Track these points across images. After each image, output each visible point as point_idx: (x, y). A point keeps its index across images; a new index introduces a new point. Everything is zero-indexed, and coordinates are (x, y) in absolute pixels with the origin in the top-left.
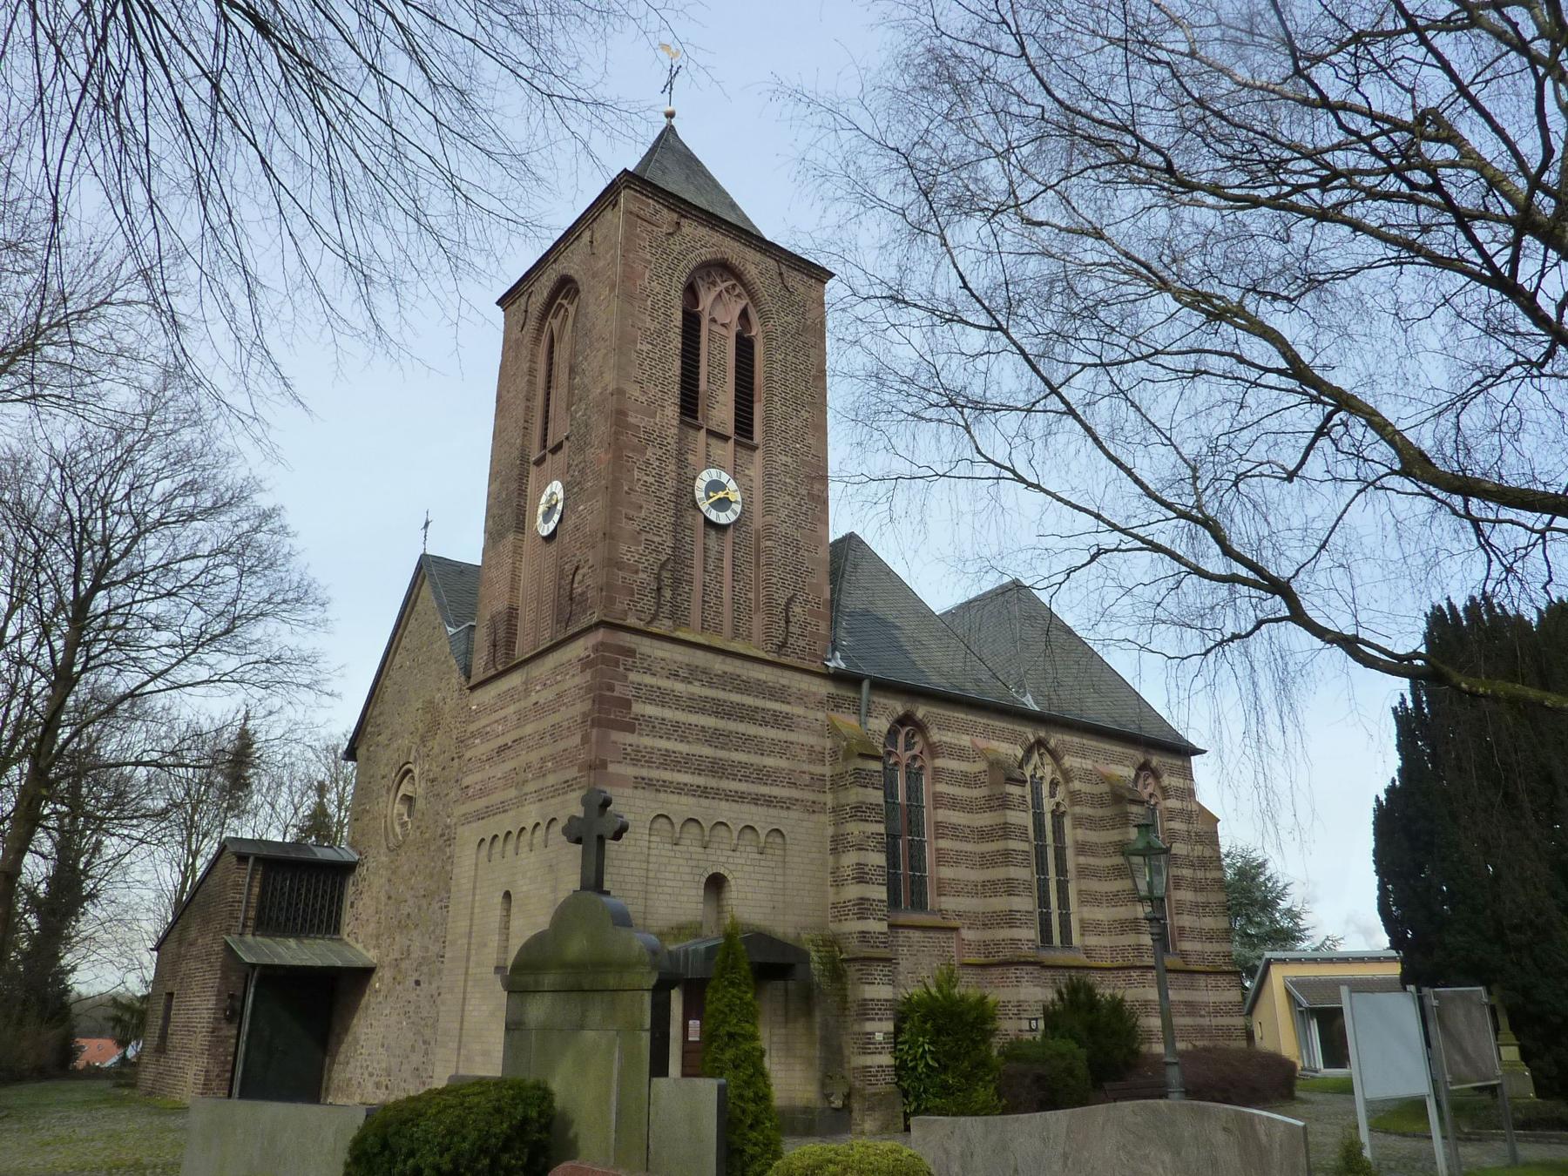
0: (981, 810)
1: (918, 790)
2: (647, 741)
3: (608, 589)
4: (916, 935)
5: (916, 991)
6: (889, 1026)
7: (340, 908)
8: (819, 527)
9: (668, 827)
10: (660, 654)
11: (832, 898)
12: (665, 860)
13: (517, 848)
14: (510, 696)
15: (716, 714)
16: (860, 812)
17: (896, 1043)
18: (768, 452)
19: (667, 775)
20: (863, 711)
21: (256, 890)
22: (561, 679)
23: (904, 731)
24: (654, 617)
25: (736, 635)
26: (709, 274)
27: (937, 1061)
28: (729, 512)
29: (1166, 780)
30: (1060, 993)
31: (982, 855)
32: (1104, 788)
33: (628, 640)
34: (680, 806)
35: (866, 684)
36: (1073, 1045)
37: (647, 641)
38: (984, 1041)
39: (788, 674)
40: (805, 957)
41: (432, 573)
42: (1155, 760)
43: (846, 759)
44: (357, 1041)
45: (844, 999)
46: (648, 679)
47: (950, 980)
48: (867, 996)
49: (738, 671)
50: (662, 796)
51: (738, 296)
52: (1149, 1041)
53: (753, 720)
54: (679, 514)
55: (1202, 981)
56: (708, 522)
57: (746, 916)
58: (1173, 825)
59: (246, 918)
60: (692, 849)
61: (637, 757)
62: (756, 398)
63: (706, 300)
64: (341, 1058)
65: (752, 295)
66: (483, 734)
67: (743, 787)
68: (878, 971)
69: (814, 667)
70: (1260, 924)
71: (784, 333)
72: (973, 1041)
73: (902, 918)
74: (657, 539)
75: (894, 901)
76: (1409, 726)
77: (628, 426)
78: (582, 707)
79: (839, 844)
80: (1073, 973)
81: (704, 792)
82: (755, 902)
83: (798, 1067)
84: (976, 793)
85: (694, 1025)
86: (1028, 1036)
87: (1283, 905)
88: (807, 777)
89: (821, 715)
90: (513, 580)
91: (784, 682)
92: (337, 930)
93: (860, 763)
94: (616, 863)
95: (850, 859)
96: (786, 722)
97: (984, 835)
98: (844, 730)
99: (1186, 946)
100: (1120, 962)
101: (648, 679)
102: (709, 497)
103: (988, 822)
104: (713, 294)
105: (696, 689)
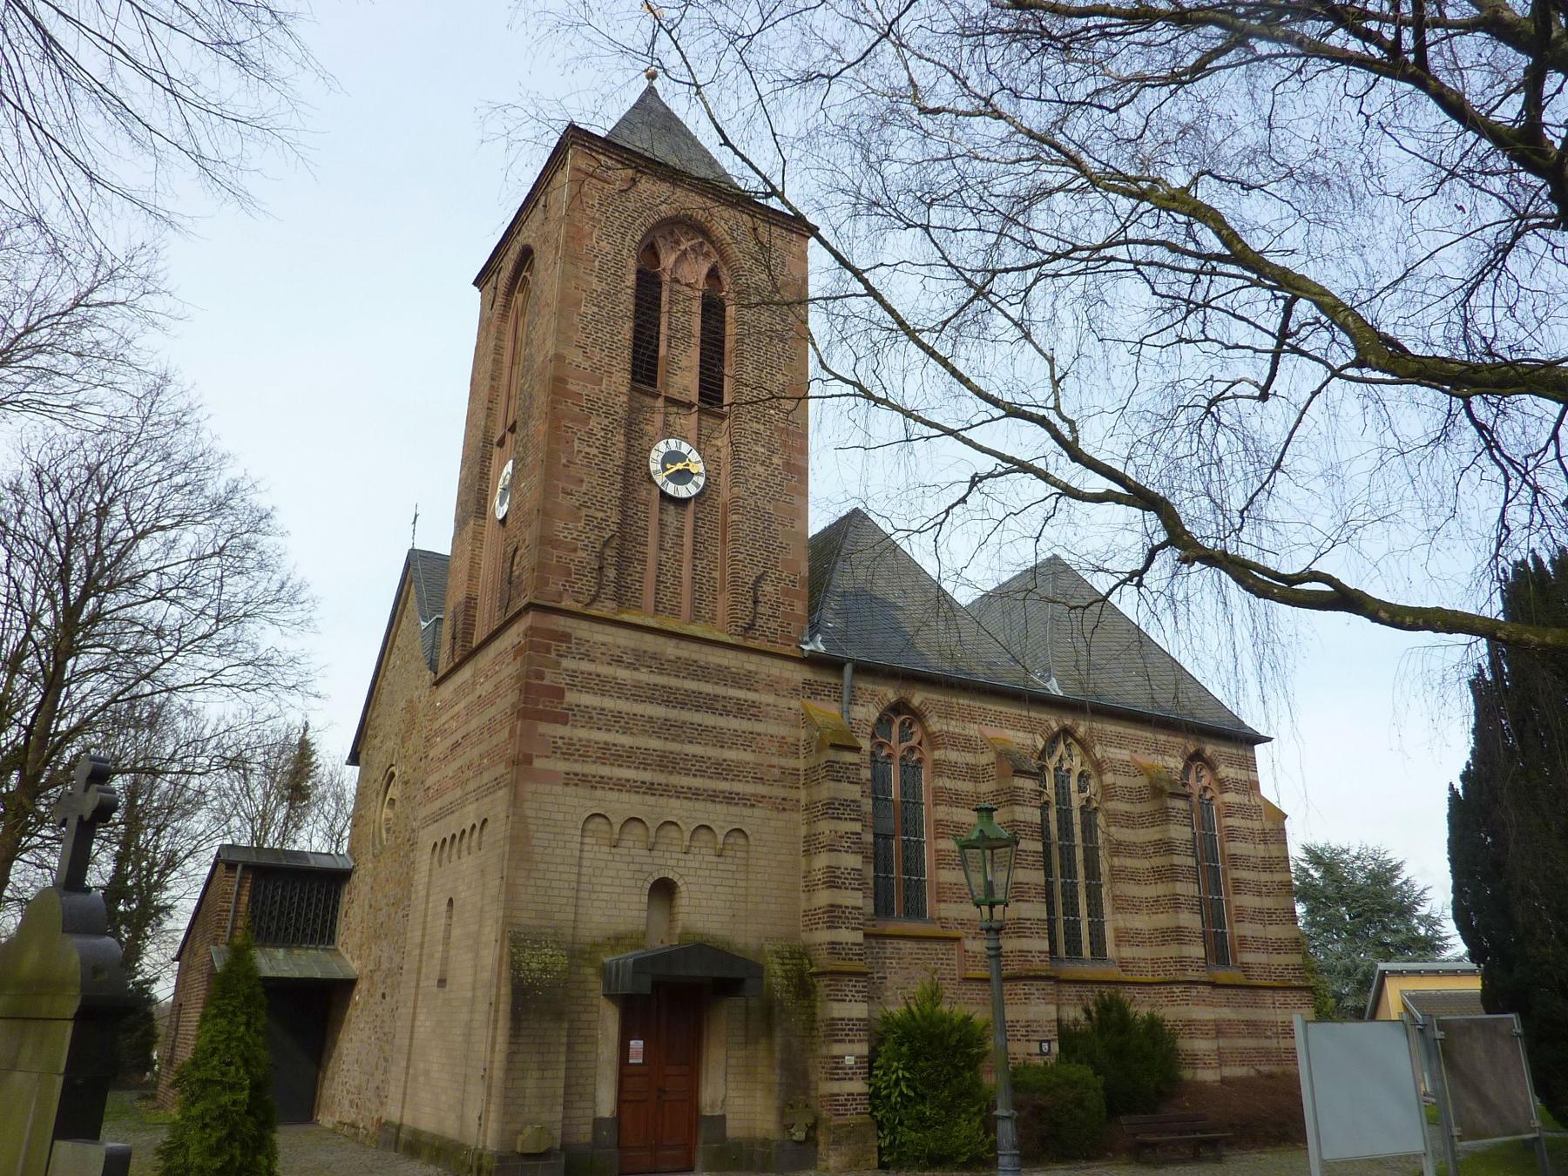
1: (917, 786)
2: (583, 733)
3: (541, 568)
4: (907, 946)
5: (897, 1010)
6: (864, 1049)
7: (334, 917)
9: (606, 828)
10: (600, 638)
11: (804, 906)
12: (602, 864)
13: (459, 851)
14: (461, 692)
15: (666, 703)
16: (834, 809)
17: (871, 1068)
19: (605, 771)
20: (846, 698)
21: (245, 899)
22: (496, 671)
23: (898, 721)
24: (595, 599)
25: (696, 616)
26: (672, 233)
27: (914, 1090)
28: (690, 485)
29: (1224, 771)
30: (1087, 1011)
32: (1142, 781)
33: (562, 623)
34: (621, 805)
35: (848, 669)
36: (1086, 1072)
37: (585, 625)
39: (755, 658)
41: (419, 567)
42: (1209, 749)
43: (819, 751)
44: (341, 1055)
45: (812, 1018)
46: (586, 666)
47: (935, 996)
48: (836, 1015)
49: (695, 656)
50: (599, 793)
51: (707, 255)
52: (1193, 1066)
53: (711, 709)
54: (626, 486)
55: (1268, 996)
56: (663, 494)
57: (700, 925)
58: (1229, 821)
59: (234, 928)
60: (633, 852)
61: (569, 751)
63: (668, 260)
64: (329, 1073)
66: (441, 732)
67: (630, 774)
68: (848, 986)
69: (787, 651)
70: (1397, 931)
72: (955, 1067)
73: (892, 927)
74: (600, 515)
75: (883, 908)
76: (1492, 701)
77: (568, 394)
78: (512, 697)
79: (812, 845)
80: (1104, 988)
81: (650, 789)
82: (712, 908)
83: (759, 1094)
85: (636, 1045)
86: (1039, 1061)
87: (1422, 911)
88: (777, 771)
89: (795, 704)
90: (472, 567)
91: (752, 668)
92: (332, 940)
93: (832, 755)
94: (542, 866)
95: (822, 860)
96: (752, 711)
98: (818, 720)
99: (1248, 957)
100: (1161, 977)
101: (586, 666)
102: (665, 469)
105: (644, 676)
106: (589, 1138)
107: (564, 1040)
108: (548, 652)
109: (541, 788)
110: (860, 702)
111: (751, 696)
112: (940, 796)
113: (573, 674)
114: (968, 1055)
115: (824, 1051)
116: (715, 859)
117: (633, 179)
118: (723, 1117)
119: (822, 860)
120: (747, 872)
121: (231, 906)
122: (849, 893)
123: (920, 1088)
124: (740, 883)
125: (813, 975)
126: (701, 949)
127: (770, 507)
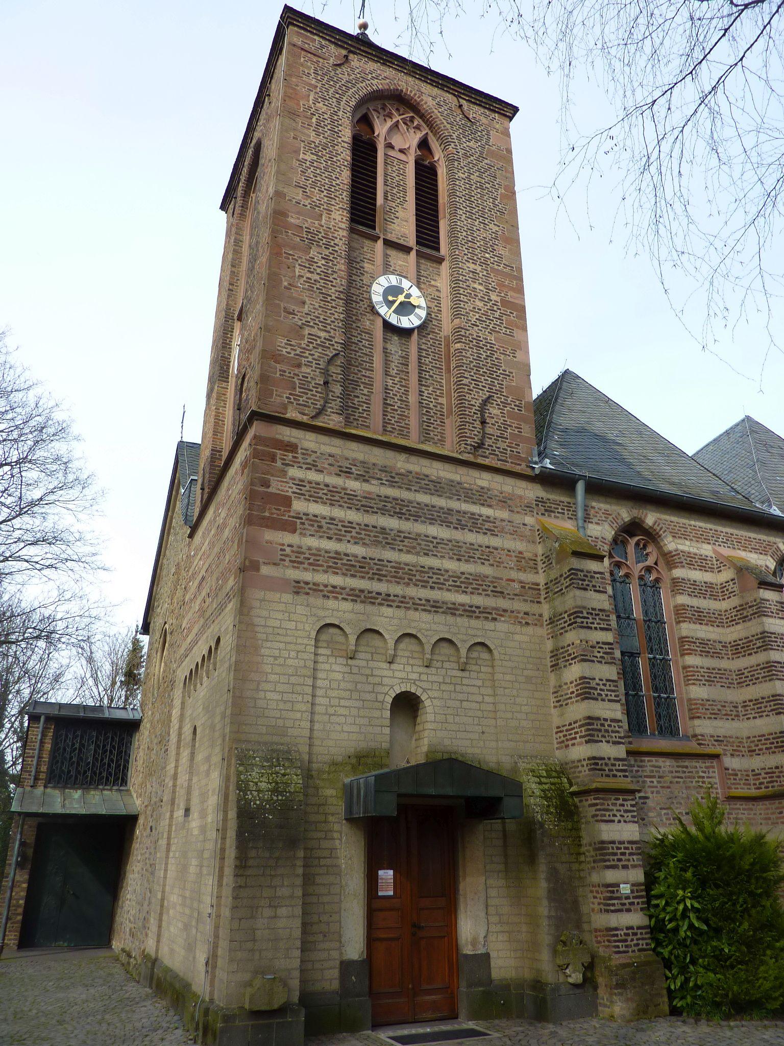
0: (733, 622)
1: (657, 604)
2: (313, 542)
4: (666, 764)
5: (668, 830)
6: (638, 875)
8: (517, 333)
11: (556, 721)
16: (580, 618)
17: (649, 898)
18: (454, 259)
21: (48, 747)
23: (633, 541)
28: (412, 317)
31: (740, 673)
33: (287, 434)
35: (580, 487)
38: (767, 894)
40: (515, 788)
41: (184, 450)
46: (313, 476)
48: (605, 837)
49: (426, 471)
51: (418, 128)
54: (349, 312)
59: (38, 772)
62: (441, 215)
63: (381, 128)
64: (120, 903)
65: (430, 124)
67: (337, 580)
68: (615, 805)
69: (521, 468)
71: (466, 156)
72: (752, 894)
73: (646, 744)
74: (323, 334)
75: (636, 726)
77: (287, 226)
79: (559, 659)
84: (724, 605)
85: (386, 875)
88: (516, 585)
89: (529, 520)
91: (484, 484)
92: (124, 782)
93: (576, 563)
95: (575, 671)
96: (487, 525)
97: (740, 648)
98: (555, 532)
101: (313, 476)
103: (743, 634)
104: (389, 123)
105: (373, 488)
106: (335, 985)
107: (300, 871)
108: (273, 459)
109: (270, 595)
110: (595, 520)
111: (486, 511)
112: (681, 613)
113: (300, 483)
114: (765, 880)
115: (595, 878)
116: (459, 674)
117: (346, 57)
118: (487, 956)
119: (575, 671)
120: (493, 687)
121: (36, 752)
122: (607, 704)
123: (713, 921)
124: (487, 699)
125: (573, 794)
126: (447, 765)
127: (492, 338)
